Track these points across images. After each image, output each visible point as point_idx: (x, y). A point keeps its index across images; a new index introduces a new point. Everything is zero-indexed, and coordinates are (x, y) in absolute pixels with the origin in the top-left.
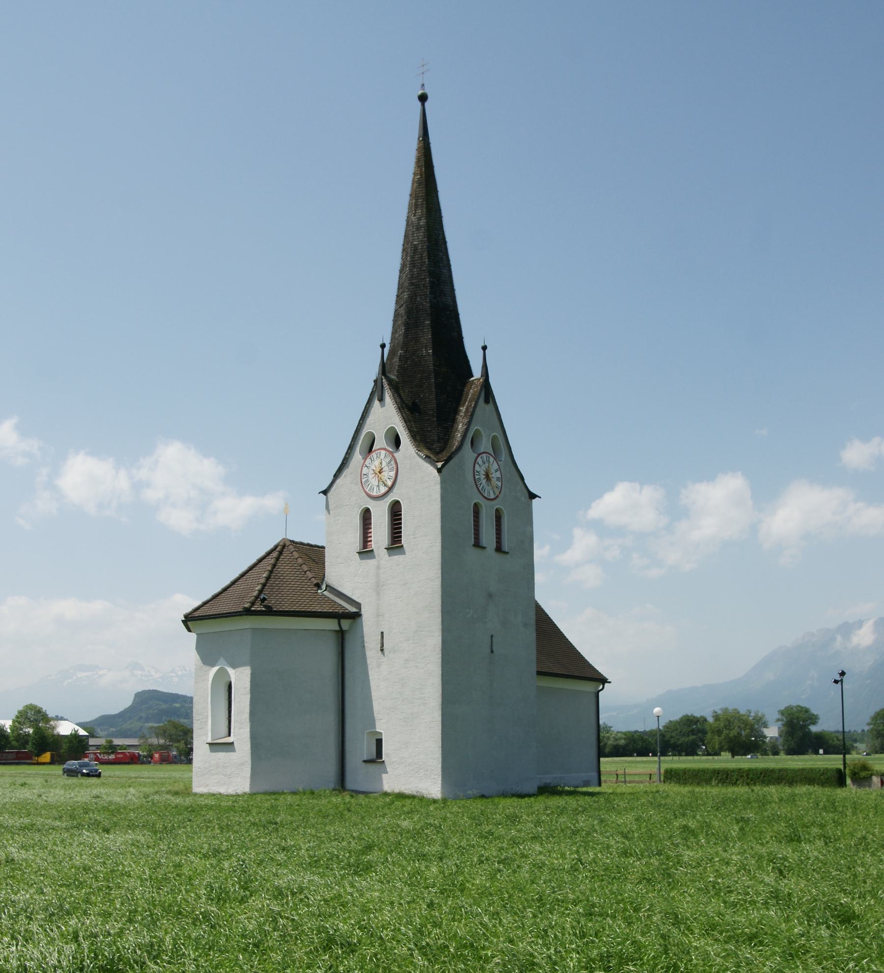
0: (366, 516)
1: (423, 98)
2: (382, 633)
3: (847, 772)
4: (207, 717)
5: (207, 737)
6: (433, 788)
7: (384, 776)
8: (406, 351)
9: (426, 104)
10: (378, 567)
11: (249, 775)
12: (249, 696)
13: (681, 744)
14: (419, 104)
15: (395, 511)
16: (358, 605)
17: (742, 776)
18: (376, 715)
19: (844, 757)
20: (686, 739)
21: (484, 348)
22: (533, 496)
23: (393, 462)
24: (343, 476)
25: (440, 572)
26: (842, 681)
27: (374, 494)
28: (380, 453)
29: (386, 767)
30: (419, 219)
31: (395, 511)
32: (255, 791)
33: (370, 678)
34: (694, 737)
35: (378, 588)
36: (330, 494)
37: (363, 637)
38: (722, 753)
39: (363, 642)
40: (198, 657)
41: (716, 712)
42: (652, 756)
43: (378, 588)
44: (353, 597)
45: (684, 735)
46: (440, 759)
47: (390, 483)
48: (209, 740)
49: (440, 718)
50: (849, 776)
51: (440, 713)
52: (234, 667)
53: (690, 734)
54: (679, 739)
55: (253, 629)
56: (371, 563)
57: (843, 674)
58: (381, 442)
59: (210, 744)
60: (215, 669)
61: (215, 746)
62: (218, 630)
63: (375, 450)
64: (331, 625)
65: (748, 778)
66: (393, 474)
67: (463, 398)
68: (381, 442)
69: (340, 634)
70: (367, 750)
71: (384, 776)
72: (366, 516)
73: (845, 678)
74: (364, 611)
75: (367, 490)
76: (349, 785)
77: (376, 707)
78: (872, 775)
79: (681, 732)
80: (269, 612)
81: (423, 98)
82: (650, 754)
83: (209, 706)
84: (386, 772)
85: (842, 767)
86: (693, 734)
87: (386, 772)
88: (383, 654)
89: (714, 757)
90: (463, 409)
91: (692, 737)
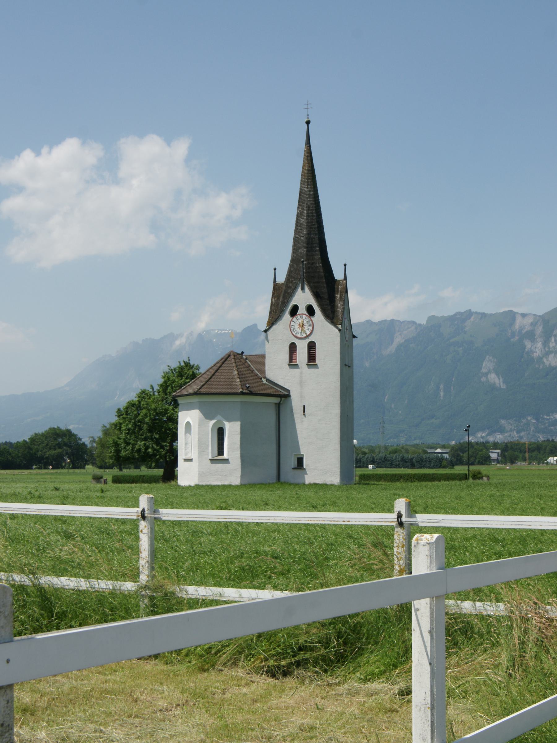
0: (293, 347)
1: (308, 123)
2: (304, 406)
3: (471, 475)
4: (208, 446)
5: (208, 454)
6: (335, 479)
7: (306, 476)
8: (308, 263)
9: (310, 125)
10: (301, 373)
11: (240, 475)
12: (239, 436)
13: (47, 458)
14: (306, 125)
15: (312, 347)
16: (289, 391)
17: (410, 478)
18: (300, 446)
19: (469, 467)
20: (53, 452)
21: (345, 265)
22: (354, 337)
23: (311, 322)
24: (278, 324)
25: (339, 379)
26: (468, 430)
27: (299, 336)
28: (302, 316)
29: (306, 471)
30: (310, 191)
31: (312, 347)
32: (243, 483)
33: (297, 427)
34: (60, 450)
35: (301, 384)
36: (268, 333)
37: (292, 407)
38: (87, 466)
39: (292, 409)
40: (201, 414)
41: (106, 427)
42: (52, 469)
43: (301, 384)
44: (285, 387)
45: (50, 449)
46: (339, 467)
47: (308, 333)
48: (210, 457)
49: (339, 448)
50: (471, 477)
51: (339, 446)
52: (229, 420)
53: (57, 447)
54: (45, 452)
55: (241, 402)
56: (295, 371)
57: (469, 426)
58: (302, 310)
59: (210, 460)
60: (213, 422)
61: (186, 460)
62: (216, 401)
63: (299, 314)
64: (276, 400)
65: (414, 478)
66: (311, 328)
67: (336, 289)
68: (302, 310)
69: (277, 406)
70: (294, 463)
71: (306, 476)
72: (293, 347)
73: (470, 429)
74: (291, 394)
75: (294, 334)
76: (282, 479)
77: (300, 442)
78: (483, 476)
79: (47, 445)
80: (251, 394)
81: (308, 123)
82: (51, 467)
83: (210, 440)
84: (307, 474)
85: (467, 472)
86: (60, 448)
87: (307, 474)
88: (305, 417)
89: (106, 470)
90: (338, 296)
91: (58, 451)
